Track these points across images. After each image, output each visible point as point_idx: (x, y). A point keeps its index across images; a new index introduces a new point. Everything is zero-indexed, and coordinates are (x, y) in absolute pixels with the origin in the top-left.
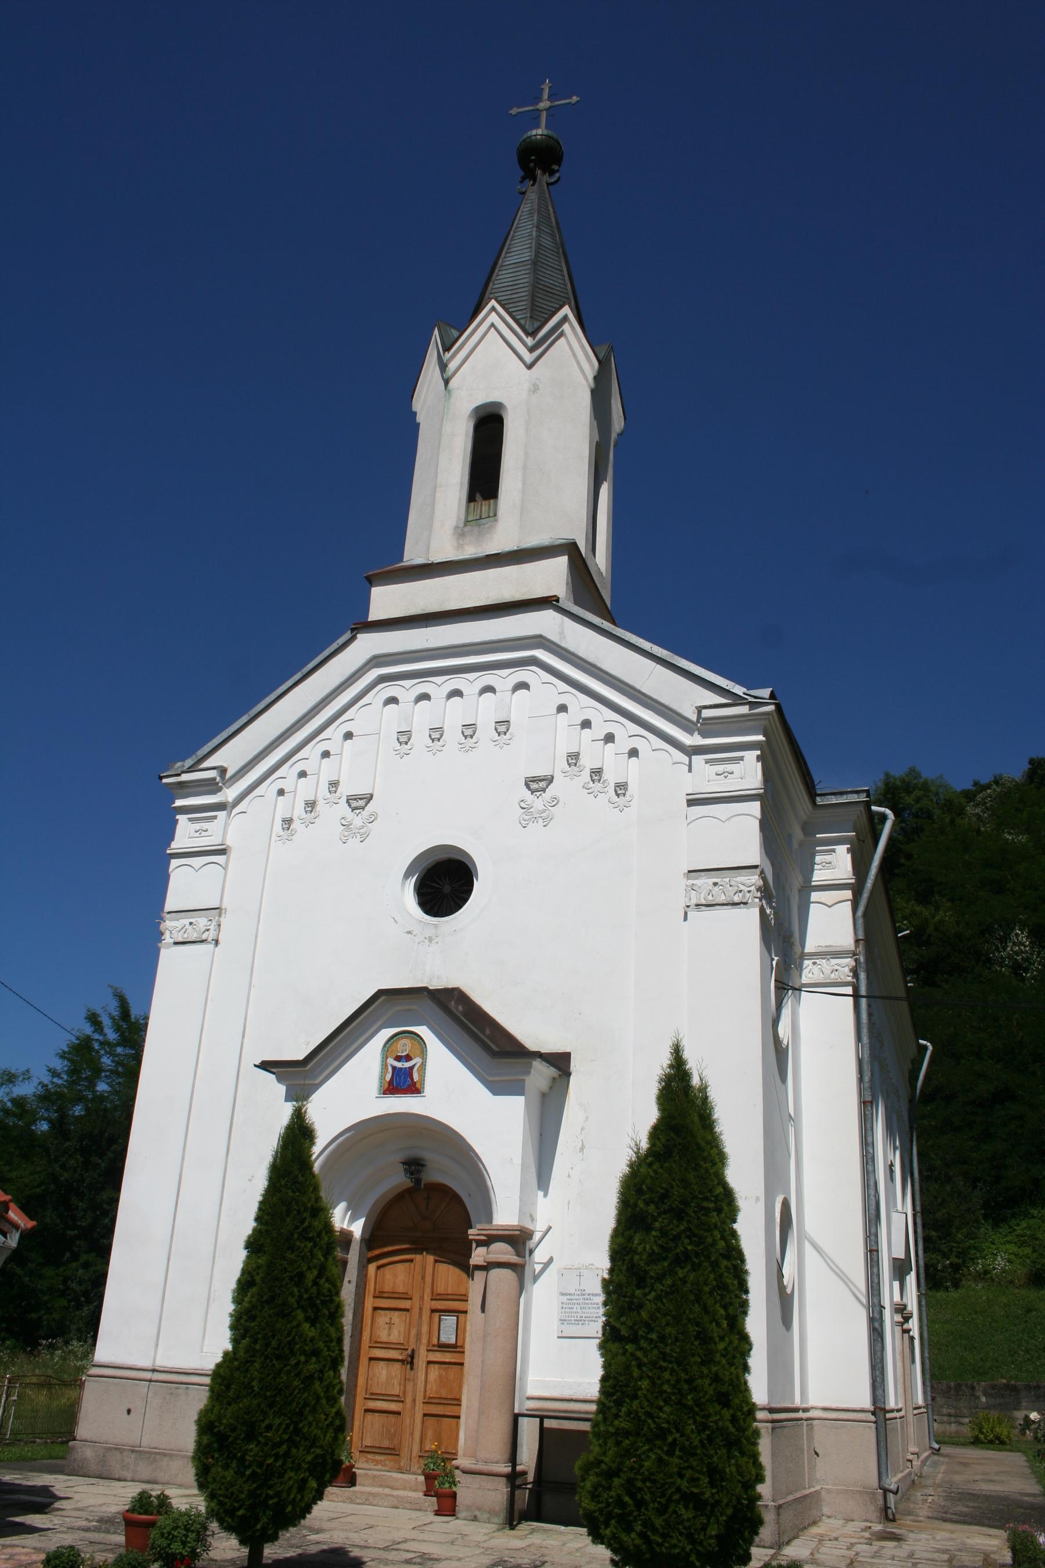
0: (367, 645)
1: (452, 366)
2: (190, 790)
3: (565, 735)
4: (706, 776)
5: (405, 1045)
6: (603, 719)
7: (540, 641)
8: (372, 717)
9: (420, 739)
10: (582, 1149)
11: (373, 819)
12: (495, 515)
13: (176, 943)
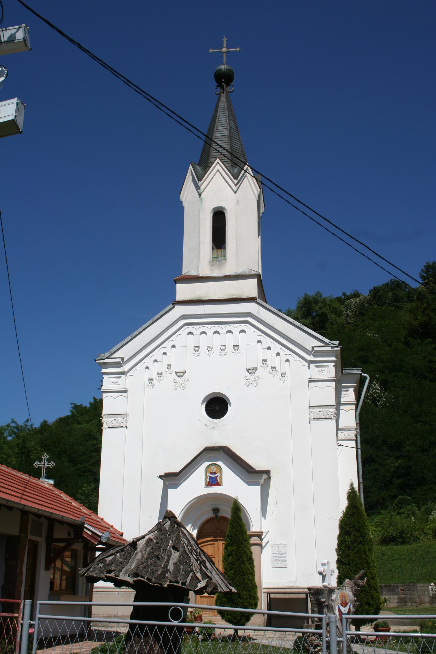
0: (179, 310)
1: (202, 188)
2: (108, 366)
3: (260, 352)
4: (316, 372)
5: (213, 468)
8: (182, 339)
9: (204, 350)
10: (276, 504)
11: (187, 380)
12: (224, 256)
13: (109, 427)
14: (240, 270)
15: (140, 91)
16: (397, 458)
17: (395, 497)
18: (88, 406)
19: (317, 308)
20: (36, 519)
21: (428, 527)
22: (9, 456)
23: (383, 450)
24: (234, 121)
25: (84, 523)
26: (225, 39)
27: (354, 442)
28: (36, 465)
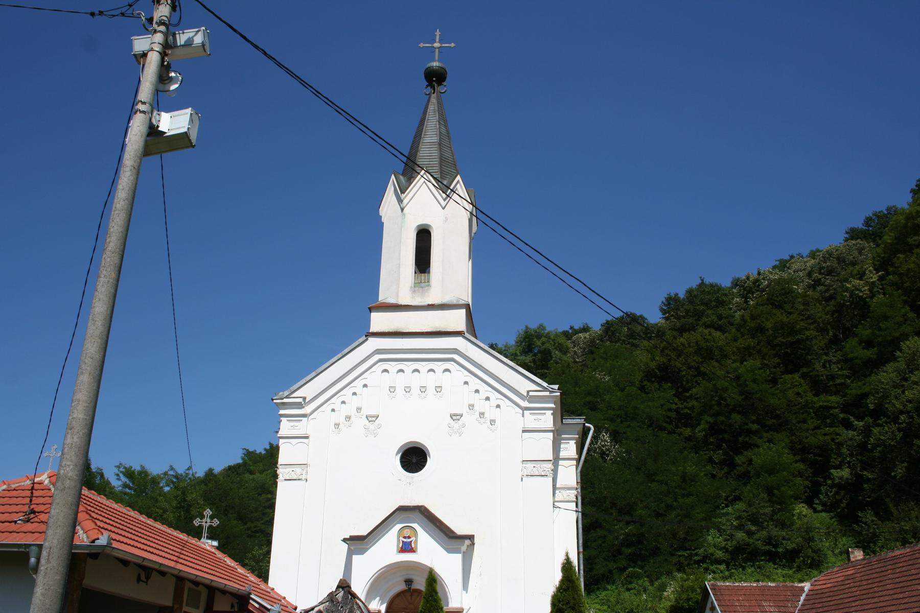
0: (373, 343)
1: (405, 202)
4: (531, 420)
6: (485, 390)
7: (455, 351)
8: (375, 377)
9: (400, 391)
11: (379, 426)
14: (446, 299)
15: (330, 103)
16: (628, 523)
17: (625, 569)
18: (263, 452)
19: (539, 343)
20: (193, 587)
21: (662, 606)
22: (165, 511)
23: (611, 514)
24: (445, 126)
25: (250, 594)
26: (438, 33)
27: (574, 504)
28: (197, 522)
